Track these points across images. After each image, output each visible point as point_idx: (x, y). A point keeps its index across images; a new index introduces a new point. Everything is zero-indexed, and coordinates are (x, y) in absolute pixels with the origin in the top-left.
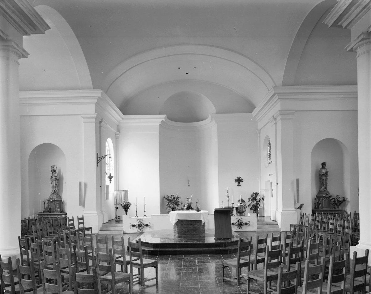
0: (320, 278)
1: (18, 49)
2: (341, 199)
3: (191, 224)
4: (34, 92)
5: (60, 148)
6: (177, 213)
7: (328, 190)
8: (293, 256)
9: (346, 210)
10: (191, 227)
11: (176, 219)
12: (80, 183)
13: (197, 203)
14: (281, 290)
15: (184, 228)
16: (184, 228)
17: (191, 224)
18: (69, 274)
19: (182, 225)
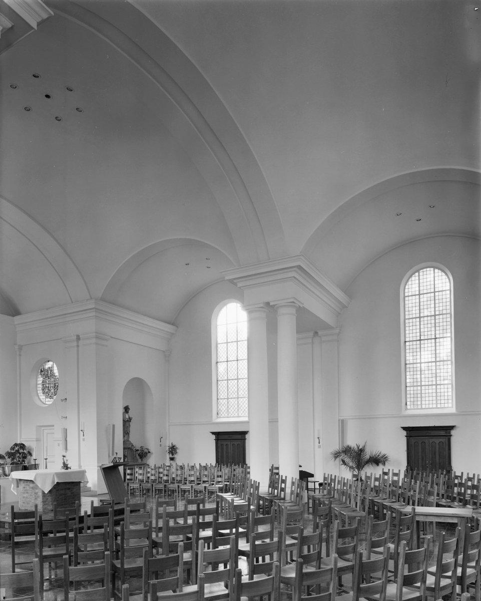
0: (386, 535)
1: (310, 287)
2: (146, 451)
3: (69, 489)
4: (145, 318)
5: (145, 380)
6: (56, 473)
7: (130, 440)
8: (162, 523)
9: (148, 463)
10: (69, 493)
11: (53, 481)
12: (53, 426)
13: (64, 456)
14: (406, 553)
15: (61, 495)
16: (61, 495)
17: (69, 489)
18: (70, 580)
19: (57, 490)
